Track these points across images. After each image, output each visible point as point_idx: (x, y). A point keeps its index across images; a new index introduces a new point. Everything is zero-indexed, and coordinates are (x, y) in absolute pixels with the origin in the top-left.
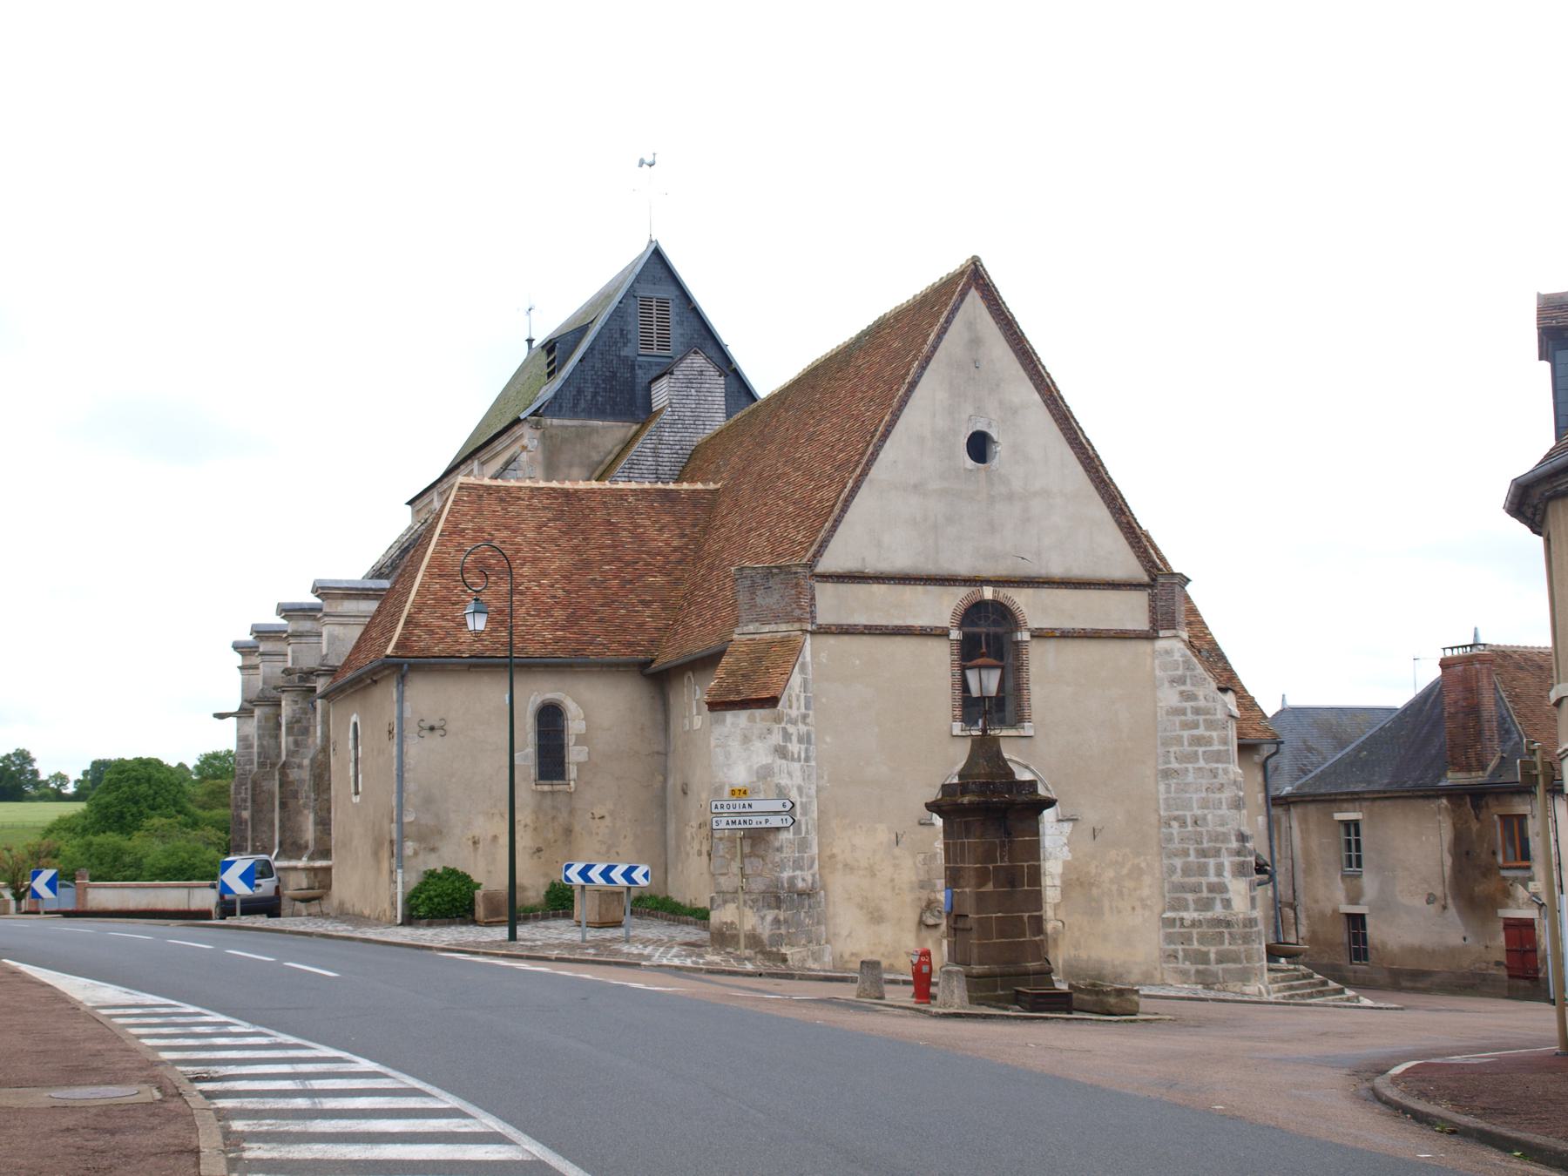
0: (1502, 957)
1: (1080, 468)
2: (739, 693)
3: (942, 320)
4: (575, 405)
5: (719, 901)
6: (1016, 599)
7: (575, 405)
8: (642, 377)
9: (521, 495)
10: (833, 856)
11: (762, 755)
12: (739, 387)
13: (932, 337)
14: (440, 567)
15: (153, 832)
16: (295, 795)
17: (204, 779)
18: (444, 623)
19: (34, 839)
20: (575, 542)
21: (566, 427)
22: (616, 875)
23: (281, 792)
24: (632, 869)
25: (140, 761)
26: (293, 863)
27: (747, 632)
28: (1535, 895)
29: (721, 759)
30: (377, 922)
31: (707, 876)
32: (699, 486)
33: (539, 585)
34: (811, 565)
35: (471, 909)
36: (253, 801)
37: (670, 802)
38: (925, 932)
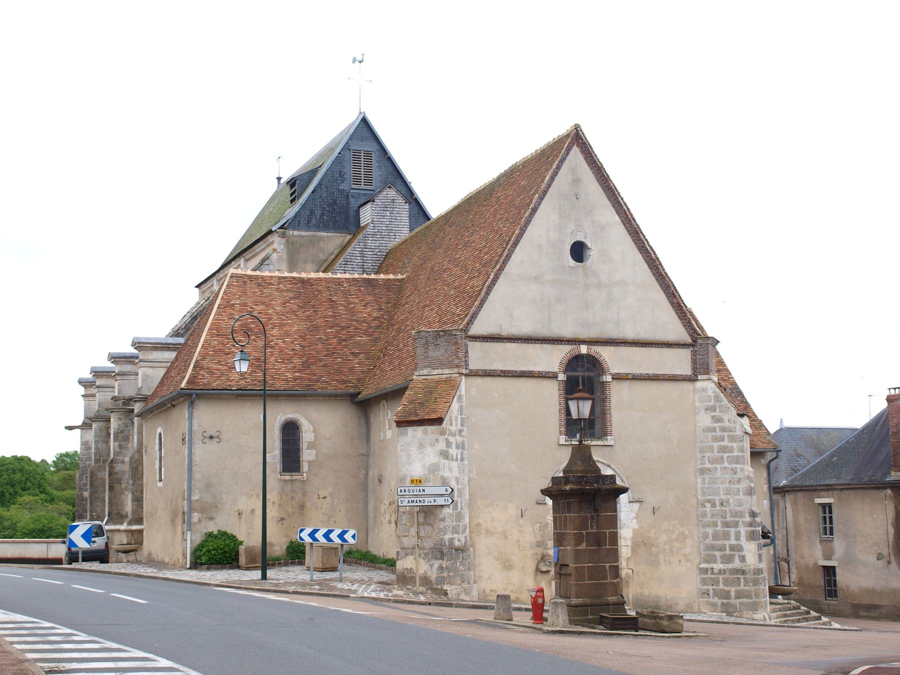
1: (646, 266)
2: (417, 415)
3: (554, 167)
4: (309, 222)
5: (402, 554)
6: (602, 353)
7: (309, 222)
8: (354, 204)
10: (479, 525)
11: (431, 456)
12: (418, 211)
13: (547, 178)
14: (217, 329)
15: (24, 505)
16: (119, 481)
18: (220, 367)
23: (110, 480)
24: (330, 532)
25: (15, 458)
26: (117, 527)
27: (423, 374)
30: (173, 566)
31: (394, 537)
32: (391, 276)
34: (465, 330)
36: (91, 485)
37: (370, 488)
38: (540, 576)
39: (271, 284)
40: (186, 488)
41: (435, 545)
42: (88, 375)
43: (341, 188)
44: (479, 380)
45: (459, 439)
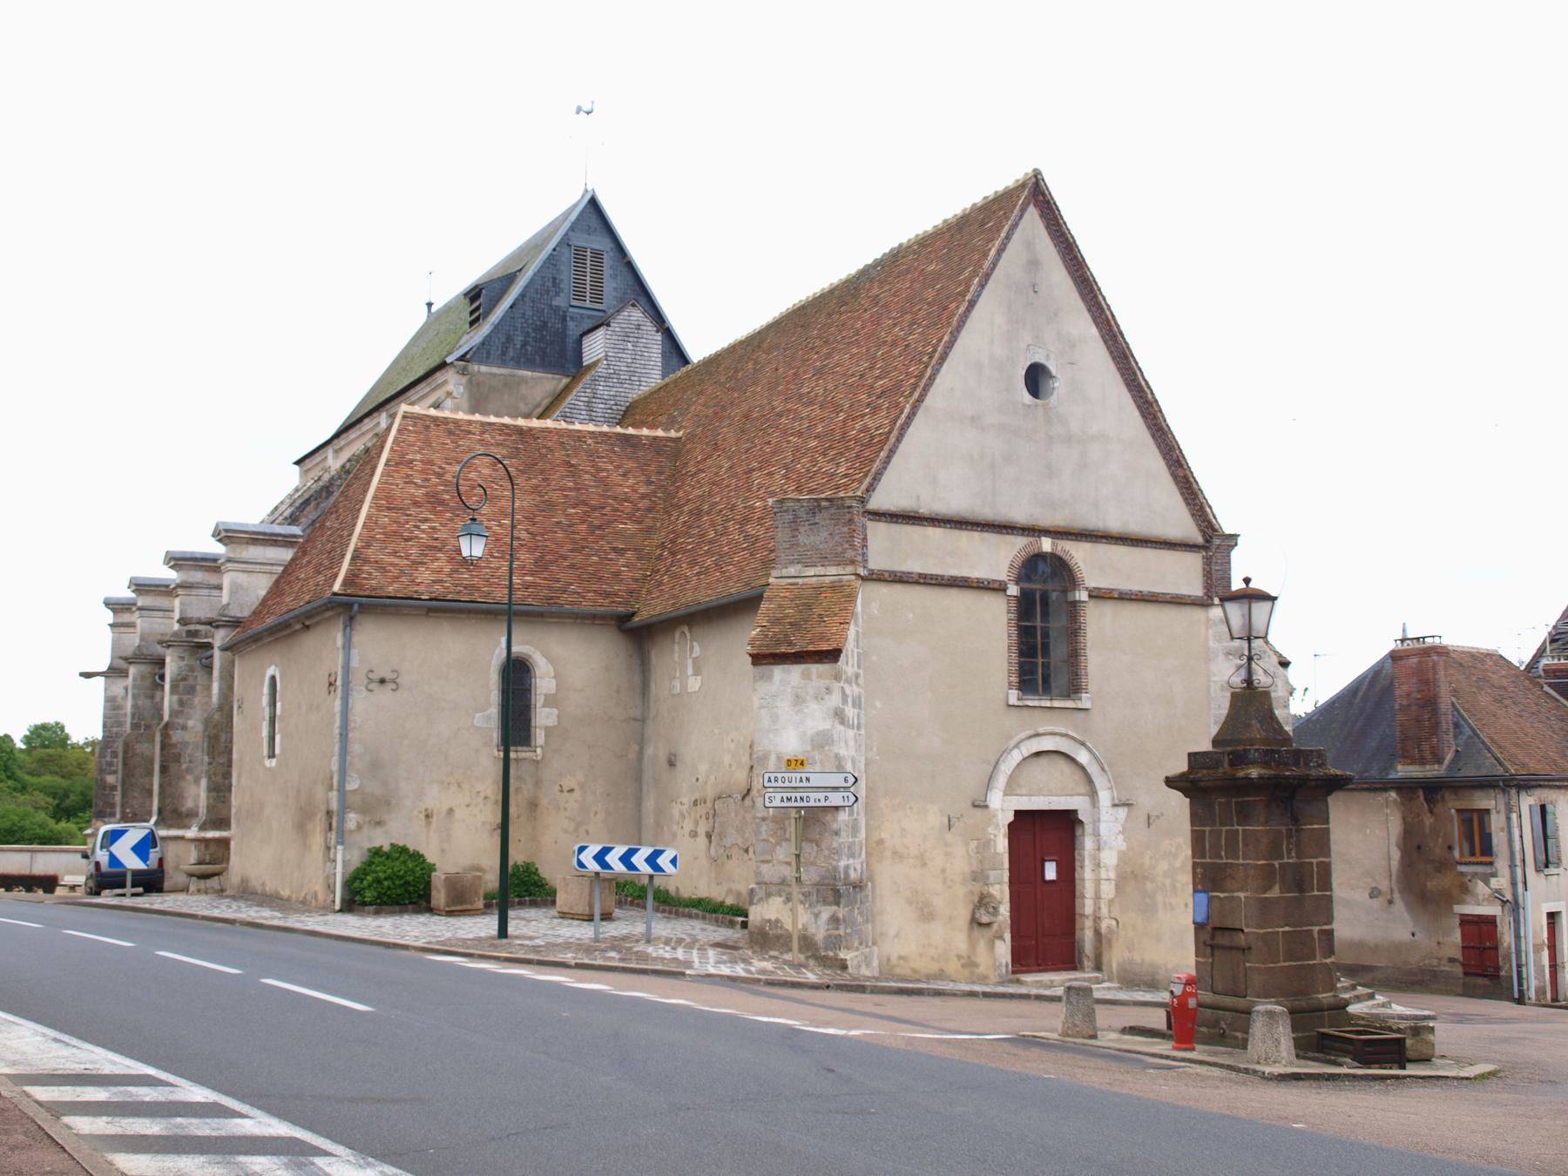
0: (1458, 954)
1: (1137, 413)
2: (790, 644)
3: (1003, 235)
4: (504, 353)
5: (760, 893)
6: (1073, 553)
7: (504, 353)
8: (573, 329)
9: (471, 428)
10: (881, 842)
11: (817, 718)
12: (674, 349)
13: (993, 252)
16: (177, 759)
17: (31, 748)
18: (396, 561)
20: (534, 481)
21: (495, 375)
23: (162, 755)
24: (606, 851)
26: (180, 833)
27: (786, 576)
28: (1497, 891)
30: (305, 906)
31: (704, 862)
32: (660, 433)
33: (500, 525)
34: (863, 500)
35: (427, 896)
36: (125, 764)
37: (647, 775)
38: (977, 932)
39: (470, 432)
41: (823, 878)
43: (554, 303)
45: (856, 690)
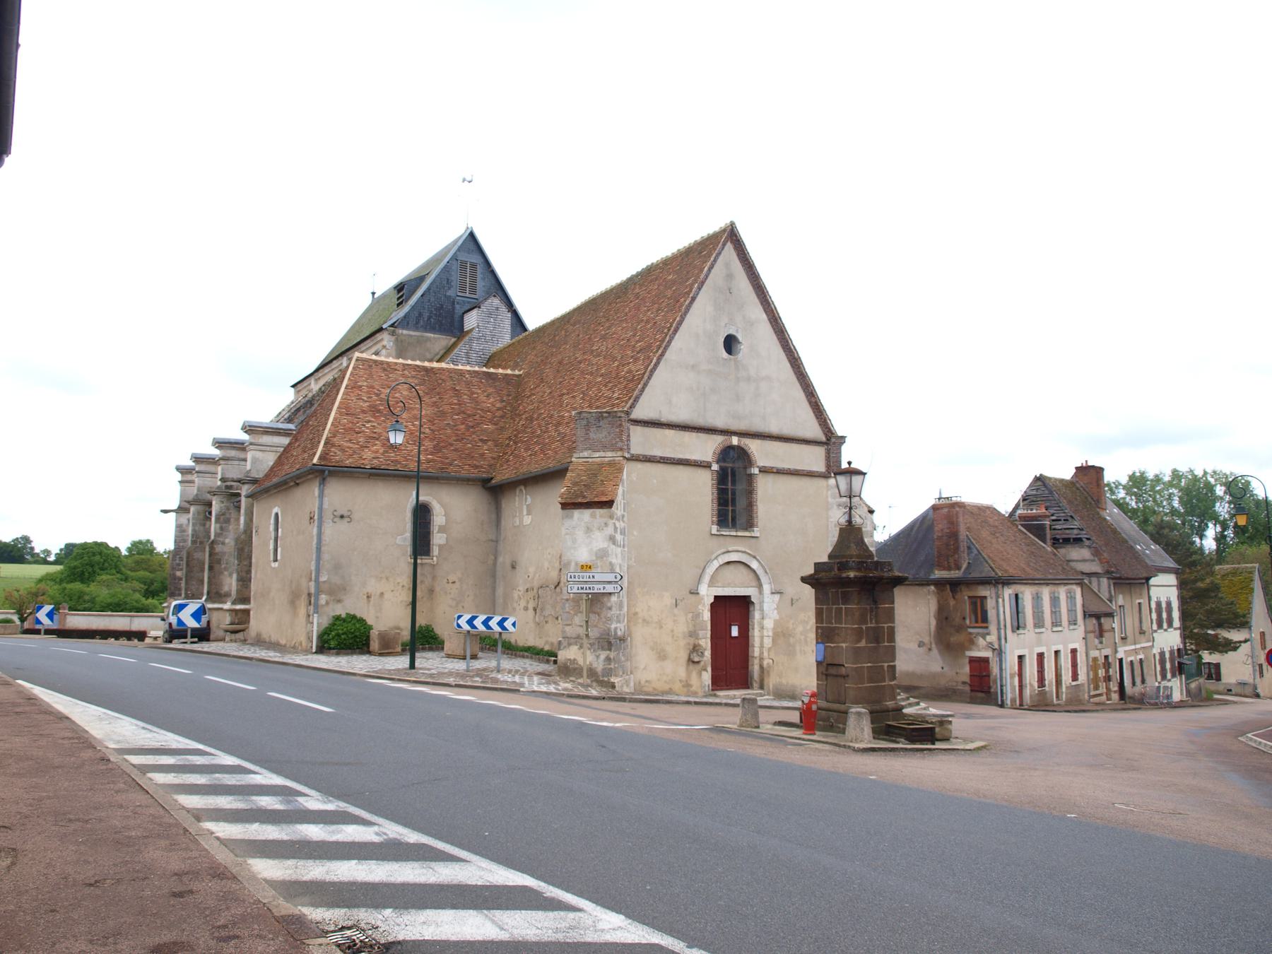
0: (968, 680)
2: (584, 497)
5: (565, 643)
8: (459, 309)
10: (636, 614)
11: (599, 541)
12: (518, 323)
14: (346, 408)
15: (102, 583)
16: (219, 562)
19: (31, 585)
22: (478, 623)
25: (96, 543)
29: (569, 543)
30: (294, 649)
31: (532, 625)
32: (509, 372)
34: (628, 413)
35: (368, 645)
36: (188, 565)
37: (499, 574)
38: (692, 667)
40: (313, 568)
42: (190, 463)
44: (639, 466)
